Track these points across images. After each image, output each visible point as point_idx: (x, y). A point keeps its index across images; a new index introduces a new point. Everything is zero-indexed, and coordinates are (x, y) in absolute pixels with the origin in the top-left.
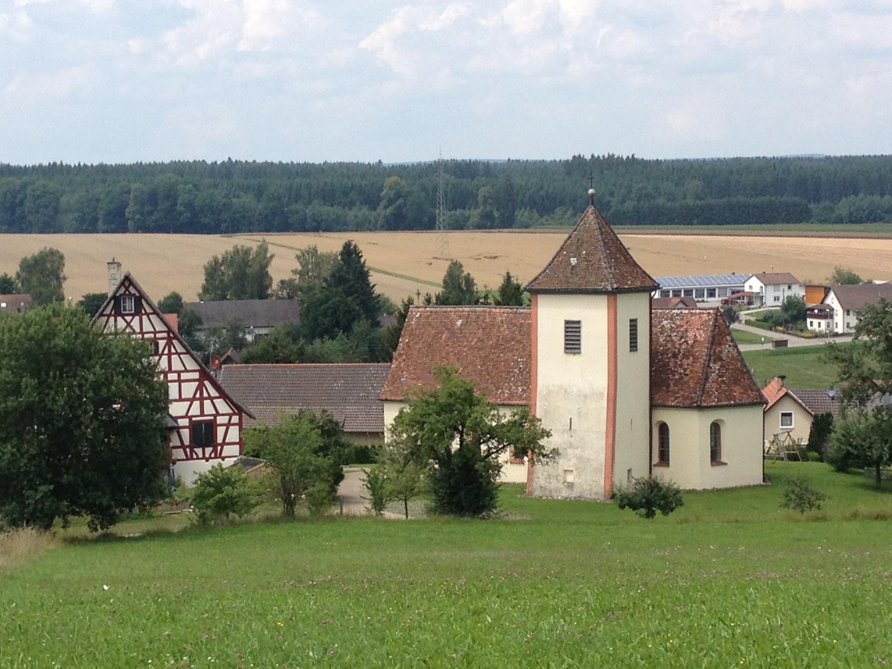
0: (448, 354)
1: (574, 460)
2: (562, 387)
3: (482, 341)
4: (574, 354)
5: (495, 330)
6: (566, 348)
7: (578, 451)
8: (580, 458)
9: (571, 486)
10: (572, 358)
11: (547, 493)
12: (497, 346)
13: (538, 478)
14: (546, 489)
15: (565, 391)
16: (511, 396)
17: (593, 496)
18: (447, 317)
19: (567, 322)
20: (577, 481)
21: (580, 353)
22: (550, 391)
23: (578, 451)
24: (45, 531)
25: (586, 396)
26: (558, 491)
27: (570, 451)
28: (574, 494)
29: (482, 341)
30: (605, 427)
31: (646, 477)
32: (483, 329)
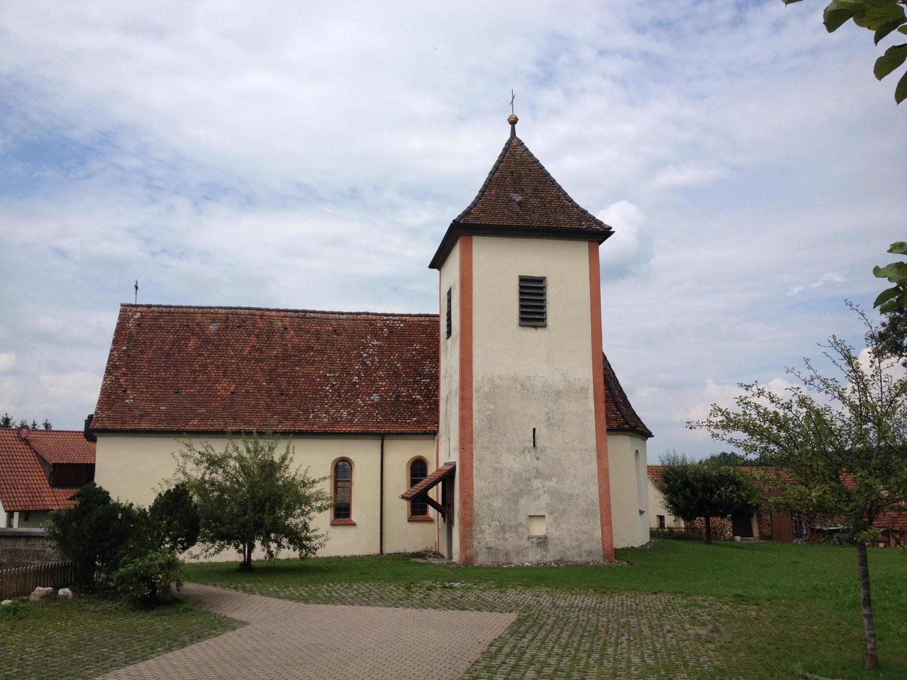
0: (205, 366)
1: (545, 499)
2: (515, 379)
3: (260, 350)
4: (535, 327)
5: (276, 338)
6: (522, 319)
7: (552, 483)
8: (555, 494)
9: (542, 542)
10: (532, 334)
11: (501, 559)
12: (286, 357)
13: (482, 532)
14: (497, 551)
15: (522, 385)
16: (335, 421)
17: (585, 558)
18: (193, 320)
19: (522, 279)
20: (553, 533)
21: (545, 326)
22: (495, 387)
23: (552, 483)
24: (704, 475)
25: (558, 393)
26: (519, 552)
27: (537, 483)
28: (551, 556)
29: (260, 350)
30: (595, 442)
31: (377, 551)
32: (257, 336)
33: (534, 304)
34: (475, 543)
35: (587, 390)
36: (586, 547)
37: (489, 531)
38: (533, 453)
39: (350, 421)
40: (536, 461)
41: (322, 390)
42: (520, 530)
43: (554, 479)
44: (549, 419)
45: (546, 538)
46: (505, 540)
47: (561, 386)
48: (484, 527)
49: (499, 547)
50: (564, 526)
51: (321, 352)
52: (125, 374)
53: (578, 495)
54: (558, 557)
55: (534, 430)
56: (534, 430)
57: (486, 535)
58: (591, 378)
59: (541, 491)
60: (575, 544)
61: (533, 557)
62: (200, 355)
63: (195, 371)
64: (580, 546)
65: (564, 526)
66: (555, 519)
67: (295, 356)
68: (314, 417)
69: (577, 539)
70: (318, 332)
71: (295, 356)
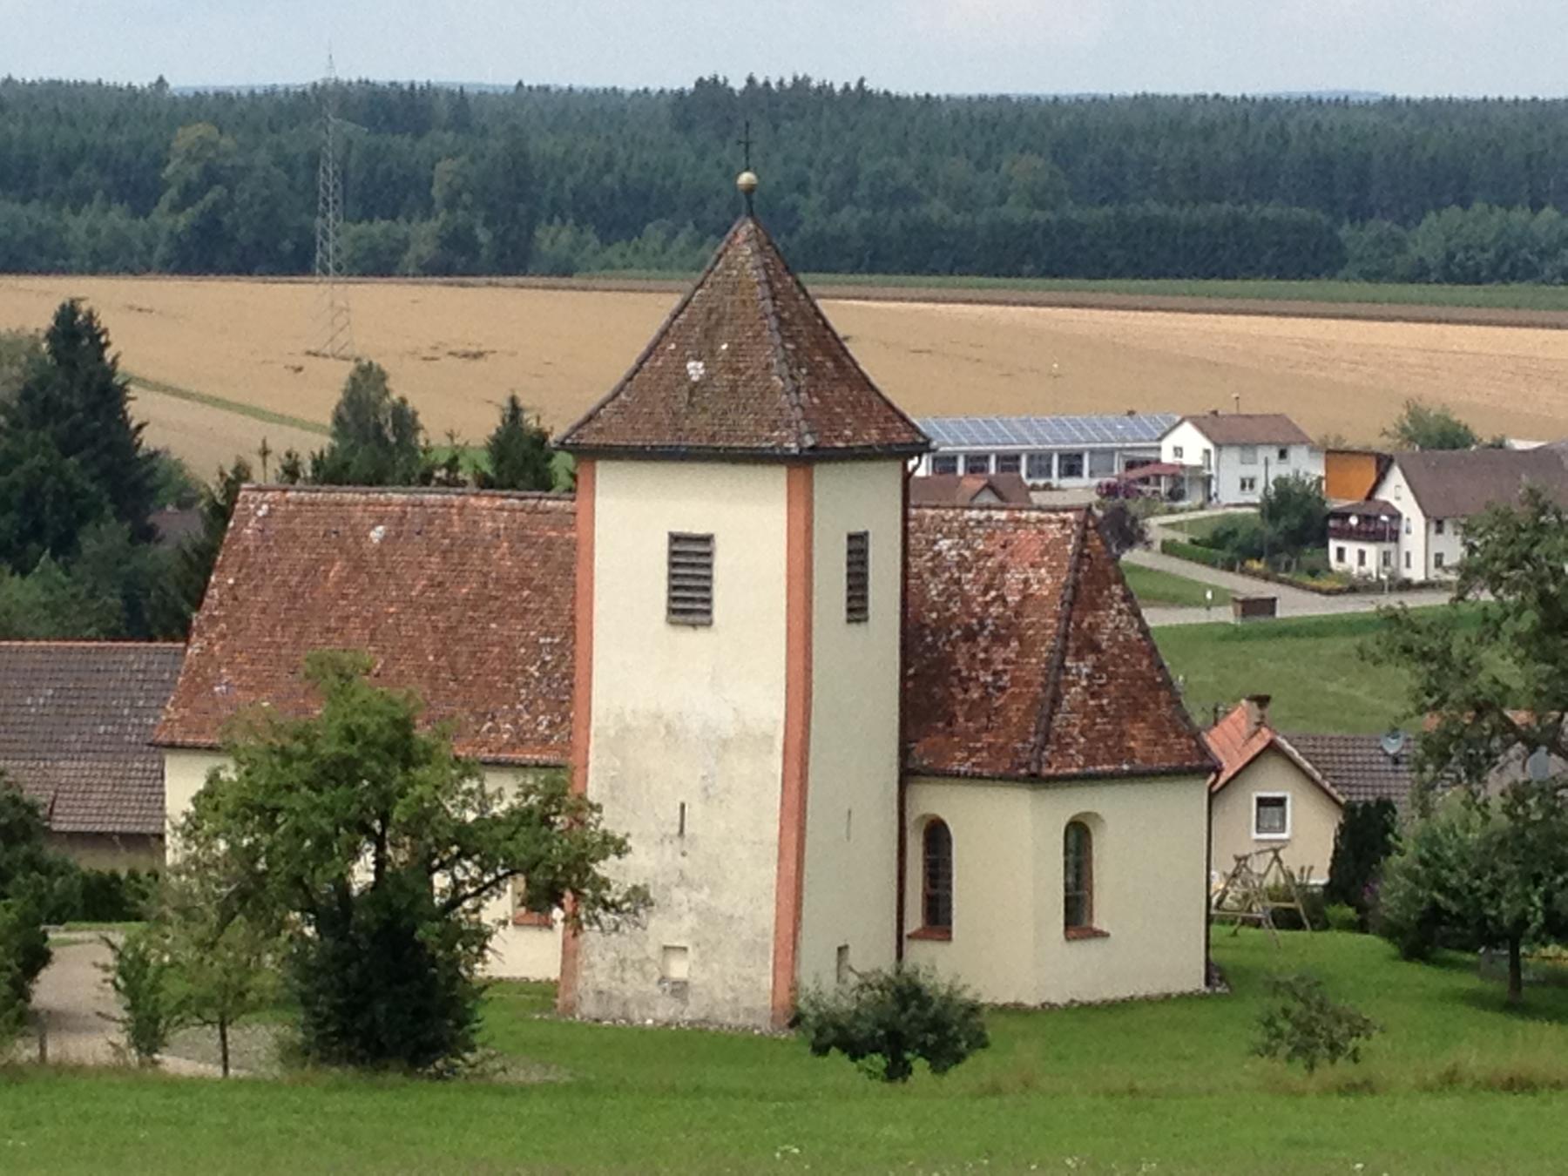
1: (690, 921)
4: (694, 625)
5: (475, 557)
7: (703, 896)
8: (707, 915)
9: (680, 989)
13: (591, 966)
15: (667, 726)
19: (675, 538)
20: (699, 978)
22: (627, 729)
23: (703, 896)
25: (725, 744)
26: (645, 1002)
27: (678, 894)
28: (691, 1011)
33: (688, 594)
34: (580, 984)
35: (772, 738)
36: (746, 1002)
37: (600, 964)
38: (677, 842)
39: (546, 740)
40: (679, 857)
41: (524, 671)
42: (648, 967)
43: (707, 890)
44: (706, 789)
45: (686, 983)
46: (623, 981)
47: (730, 731)
48: (595, 958)
49: (616, 993)
50: (715, 966)
51: (543, 590)
52: (223, 636)
53: (741, 918)
54: (702, 1015)
55: (683, 807)
56: (683, 807)
57: (596, 970)
58: (782, 717)
59: (685, 908)
60: (729, 996)
61: (664, 1010)
62: (344, 596)
63: (328, 630)
64: (736, 1000)
65: (715, 966)
66: (702, 955)
67: (497, 598)
68: (489, 730)
69: (732, 989)
70: (550, 543)
71: (497, 598)
